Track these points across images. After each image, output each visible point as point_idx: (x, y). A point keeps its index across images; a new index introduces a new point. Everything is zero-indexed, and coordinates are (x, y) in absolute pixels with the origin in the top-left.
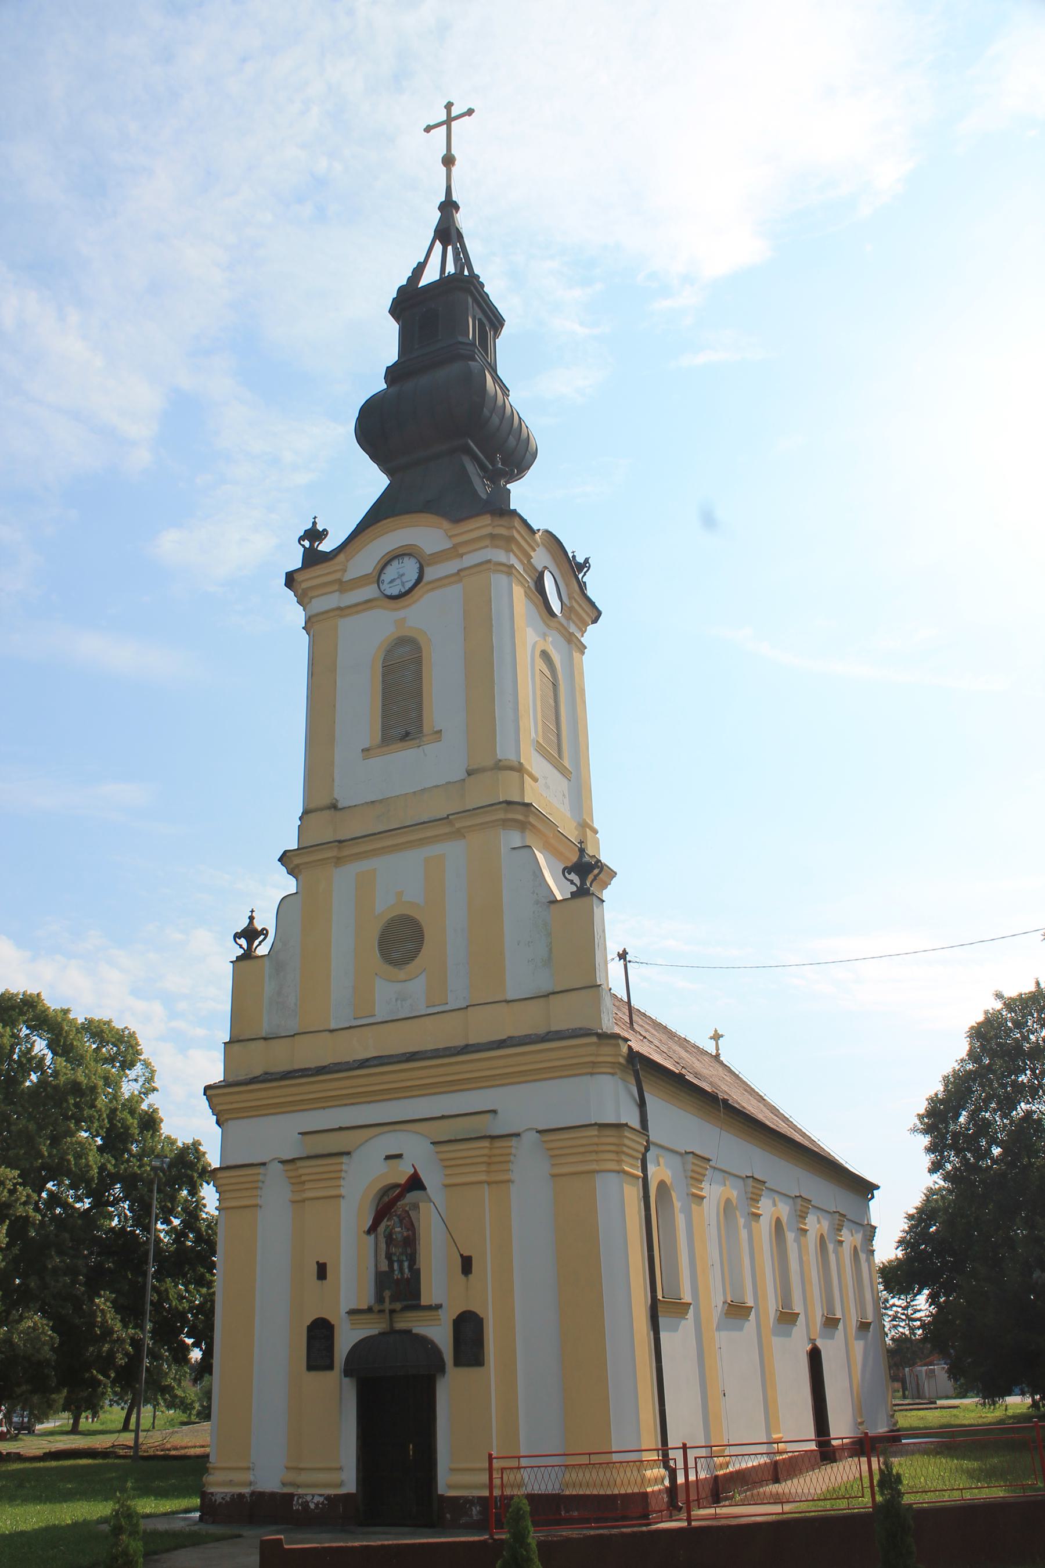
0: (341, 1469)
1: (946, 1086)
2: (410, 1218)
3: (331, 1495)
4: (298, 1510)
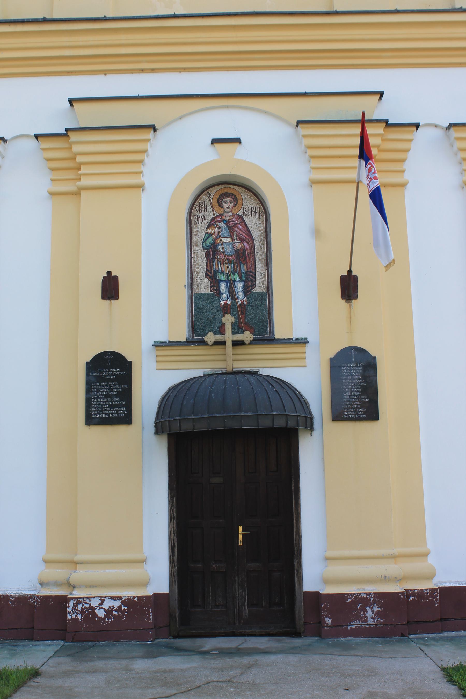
0: (144, 561)
1: (344, 299)
3: (134, 597)
4: (76, 619)
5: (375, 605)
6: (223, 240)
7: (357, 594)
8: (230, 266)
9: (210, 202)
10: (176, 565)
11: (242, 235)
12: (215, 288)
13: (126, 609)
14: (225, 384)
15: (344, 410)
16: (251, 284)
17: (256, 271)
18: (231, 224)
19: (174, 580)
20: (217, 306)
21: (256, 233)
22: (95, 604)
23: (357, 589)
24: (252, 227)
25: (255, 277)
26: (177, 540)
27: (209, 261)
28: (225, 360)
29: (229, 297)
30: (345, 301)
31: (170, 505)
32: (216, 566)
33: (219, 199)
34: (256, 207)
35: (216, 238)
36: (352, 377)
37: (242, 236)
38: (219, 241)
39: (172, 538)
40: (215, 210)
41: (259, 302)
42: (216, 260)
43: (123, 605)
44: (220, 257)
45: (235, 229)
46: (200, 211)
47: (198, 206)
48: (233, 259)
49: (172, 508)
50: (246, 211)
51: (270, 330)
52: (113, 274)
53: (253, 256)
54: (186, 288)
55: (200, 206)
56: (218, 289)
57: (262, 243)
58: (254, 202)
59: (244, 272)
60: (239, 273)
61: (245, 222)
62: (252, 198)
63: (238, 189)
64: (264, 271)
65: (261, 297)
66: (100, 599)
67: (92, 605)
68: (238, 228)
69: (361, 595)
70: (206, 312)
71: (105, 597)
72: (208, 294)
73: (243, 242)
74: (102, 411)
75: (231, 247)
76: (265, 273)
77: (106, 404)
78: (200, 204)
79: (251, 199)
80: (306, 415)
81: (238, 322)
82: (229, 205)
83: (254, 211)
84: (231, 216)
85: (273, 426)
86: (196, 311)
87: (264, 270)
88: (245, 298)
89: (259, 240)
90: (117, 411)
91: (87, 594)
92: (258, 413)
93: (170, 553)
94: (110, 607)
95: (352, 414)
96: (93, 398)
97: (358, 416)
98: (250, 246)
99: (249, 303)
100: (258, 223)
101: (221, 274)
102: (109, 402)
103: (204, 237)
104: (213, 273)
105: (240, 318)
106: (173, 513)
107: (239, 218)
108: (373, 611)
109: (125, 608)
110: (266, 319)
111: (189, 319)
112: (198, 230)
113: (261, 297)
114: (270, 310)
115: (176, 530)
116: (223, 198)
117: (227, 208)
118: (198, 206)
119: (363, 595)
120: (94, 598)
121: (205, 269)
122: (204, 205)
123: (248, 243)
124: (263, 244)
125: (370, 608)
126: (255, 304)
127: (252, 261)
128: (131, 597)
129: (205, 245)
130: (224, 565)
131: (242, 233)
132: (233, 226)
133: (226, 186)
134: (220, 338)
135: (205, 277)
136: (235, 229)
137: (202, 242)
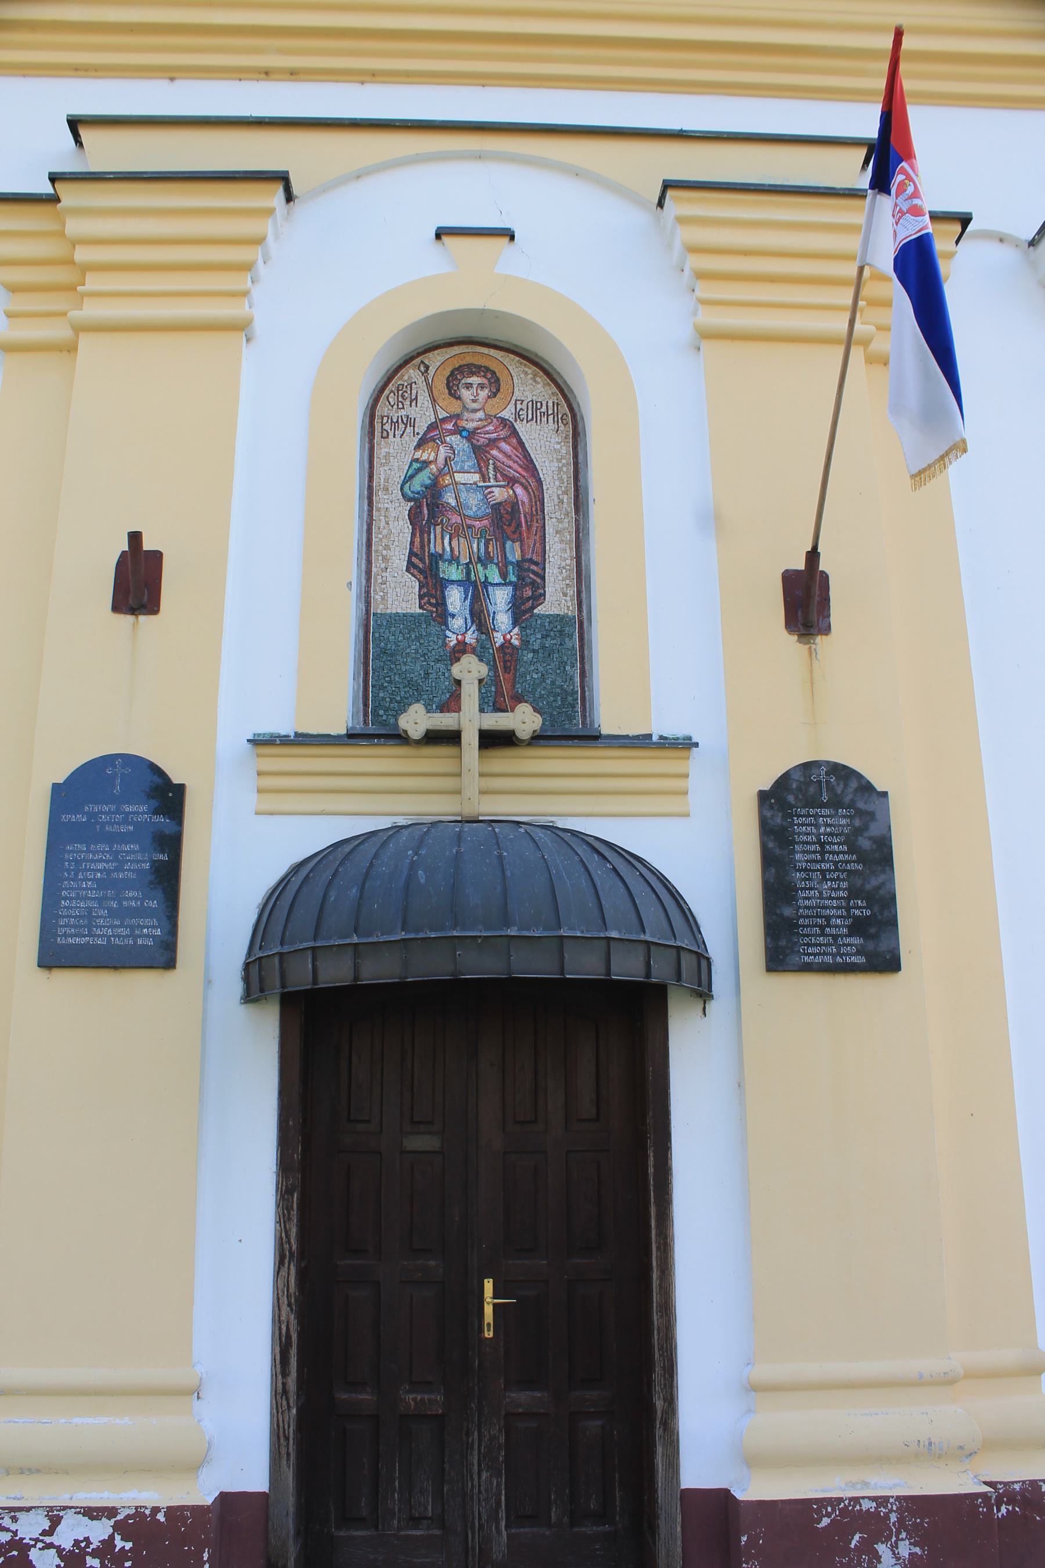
1: (795, 631)
2: (521, 444)
3: (156, 1510)
5: (903, 1535)
6: (458, 477)
7: (847, 1502)
8: (475, 546)
9: (427, 384)
10: (291, 1404)
11: (510, 467)
12: (433, 601)
13: (127, 1548)
14: (460, 842)
15: (802, 940)
16: (532, 593)
17: (547, 561)
18: (482, 440)
19: (284, 1450)
20: (436, 647)
21: (547, 463)
22: (30, 1532)
23: (846, 1484)
24: (538, 448)
25: (545, 577)
26: (299, 1323)
27: (418, 530)
28: (459, 792)
29: (472, 624)
30: (796, 637)
31: (281, 1217)
32: (414, 1399)
33: (451, 379)
34: (547, 402)
35: (440, 473)
36: (822, 845)
37: (511, 470)
38: (447, 482)
39: (283, 1318)
40: (440, 405)
41: (555, 642)
42: (439, 528)
43: (120, 1536)
44: (449, 520)
45: (491, 452)
46: (398, 405)
47: (395, 395)
48: (485, 527)
49: (285, 1226)
50: (521, 409)
51: (584, 716)
52: (147, 546)
53: (539, 521)
54: (351, 590)
55: (400, 394)
56: (442, 603)
57: (563, 489)
58: (543, 390)
59: (513, 562)
60: (500, 565)
61: (520, 437)
62: (538, 379)
63: (502, 357)
64: (568, 562)
65: (559, 627)
66: (46, 1516)
67: (20, 1535)
68: (500, 450)
69: (861, 1506)
70: (405, 664)
71: (65, 1508)
72: (412, 615)
73: (513, 485)
74: (90, 927)
75: (480, 497)
76: (572, 566)
77: (101, 907)
78: (400, 389)
79: (535, 381)
80: (699, 948)
81: (493, 694)
82: (478, 394)
83: (542, 410)
84: (480, 420)
85: (608, 973)
86: (377, 661)
87: (569, 558)
88: (516, 630)
89: (556, 483)
90: (132, 928)
91: (7, 1498)
92: (564, 932)
93: (275, 1366)
94: (77, 1543)
95: (825, 954)
96: (66, 889)
97: (843, 959)
98: (532, 495)
99: (525, 643)
100: (553, 441)
101: (450, 562)
102: (112, 900)
103: (408, 470)
104: (427, 561)
105: (499, 683)
106: (289, 1242)
107: (502, 425)
108: (896, 1558)
109: (124, 1546)
110: (574, 688)
111: (358, 680)
112: (392, 451)
113: (559, 627)
114: (584, 664)
115: (295, 1293)
116: (460, 376)
117: (472, 400)
118: (395, 395)
119: (866, 1505)
120: (28, 1512)
121: (408, 551)
122: (411, 392)
123: (525, 488)
124: (565, 493)
125: (889, 1546)
126: (543, 647)
127: (536, 535)
128: (146, 1508)
129: (410, 489)
130: (439, 1397)
131: (511, 463)
132: (487, 445)
133: (470, 348)
134: (444, 721)
135: (406, 571)
136: (491, 452)
137: (401, 482)
